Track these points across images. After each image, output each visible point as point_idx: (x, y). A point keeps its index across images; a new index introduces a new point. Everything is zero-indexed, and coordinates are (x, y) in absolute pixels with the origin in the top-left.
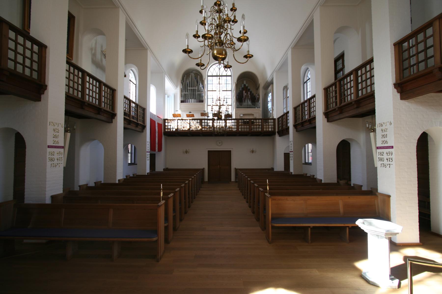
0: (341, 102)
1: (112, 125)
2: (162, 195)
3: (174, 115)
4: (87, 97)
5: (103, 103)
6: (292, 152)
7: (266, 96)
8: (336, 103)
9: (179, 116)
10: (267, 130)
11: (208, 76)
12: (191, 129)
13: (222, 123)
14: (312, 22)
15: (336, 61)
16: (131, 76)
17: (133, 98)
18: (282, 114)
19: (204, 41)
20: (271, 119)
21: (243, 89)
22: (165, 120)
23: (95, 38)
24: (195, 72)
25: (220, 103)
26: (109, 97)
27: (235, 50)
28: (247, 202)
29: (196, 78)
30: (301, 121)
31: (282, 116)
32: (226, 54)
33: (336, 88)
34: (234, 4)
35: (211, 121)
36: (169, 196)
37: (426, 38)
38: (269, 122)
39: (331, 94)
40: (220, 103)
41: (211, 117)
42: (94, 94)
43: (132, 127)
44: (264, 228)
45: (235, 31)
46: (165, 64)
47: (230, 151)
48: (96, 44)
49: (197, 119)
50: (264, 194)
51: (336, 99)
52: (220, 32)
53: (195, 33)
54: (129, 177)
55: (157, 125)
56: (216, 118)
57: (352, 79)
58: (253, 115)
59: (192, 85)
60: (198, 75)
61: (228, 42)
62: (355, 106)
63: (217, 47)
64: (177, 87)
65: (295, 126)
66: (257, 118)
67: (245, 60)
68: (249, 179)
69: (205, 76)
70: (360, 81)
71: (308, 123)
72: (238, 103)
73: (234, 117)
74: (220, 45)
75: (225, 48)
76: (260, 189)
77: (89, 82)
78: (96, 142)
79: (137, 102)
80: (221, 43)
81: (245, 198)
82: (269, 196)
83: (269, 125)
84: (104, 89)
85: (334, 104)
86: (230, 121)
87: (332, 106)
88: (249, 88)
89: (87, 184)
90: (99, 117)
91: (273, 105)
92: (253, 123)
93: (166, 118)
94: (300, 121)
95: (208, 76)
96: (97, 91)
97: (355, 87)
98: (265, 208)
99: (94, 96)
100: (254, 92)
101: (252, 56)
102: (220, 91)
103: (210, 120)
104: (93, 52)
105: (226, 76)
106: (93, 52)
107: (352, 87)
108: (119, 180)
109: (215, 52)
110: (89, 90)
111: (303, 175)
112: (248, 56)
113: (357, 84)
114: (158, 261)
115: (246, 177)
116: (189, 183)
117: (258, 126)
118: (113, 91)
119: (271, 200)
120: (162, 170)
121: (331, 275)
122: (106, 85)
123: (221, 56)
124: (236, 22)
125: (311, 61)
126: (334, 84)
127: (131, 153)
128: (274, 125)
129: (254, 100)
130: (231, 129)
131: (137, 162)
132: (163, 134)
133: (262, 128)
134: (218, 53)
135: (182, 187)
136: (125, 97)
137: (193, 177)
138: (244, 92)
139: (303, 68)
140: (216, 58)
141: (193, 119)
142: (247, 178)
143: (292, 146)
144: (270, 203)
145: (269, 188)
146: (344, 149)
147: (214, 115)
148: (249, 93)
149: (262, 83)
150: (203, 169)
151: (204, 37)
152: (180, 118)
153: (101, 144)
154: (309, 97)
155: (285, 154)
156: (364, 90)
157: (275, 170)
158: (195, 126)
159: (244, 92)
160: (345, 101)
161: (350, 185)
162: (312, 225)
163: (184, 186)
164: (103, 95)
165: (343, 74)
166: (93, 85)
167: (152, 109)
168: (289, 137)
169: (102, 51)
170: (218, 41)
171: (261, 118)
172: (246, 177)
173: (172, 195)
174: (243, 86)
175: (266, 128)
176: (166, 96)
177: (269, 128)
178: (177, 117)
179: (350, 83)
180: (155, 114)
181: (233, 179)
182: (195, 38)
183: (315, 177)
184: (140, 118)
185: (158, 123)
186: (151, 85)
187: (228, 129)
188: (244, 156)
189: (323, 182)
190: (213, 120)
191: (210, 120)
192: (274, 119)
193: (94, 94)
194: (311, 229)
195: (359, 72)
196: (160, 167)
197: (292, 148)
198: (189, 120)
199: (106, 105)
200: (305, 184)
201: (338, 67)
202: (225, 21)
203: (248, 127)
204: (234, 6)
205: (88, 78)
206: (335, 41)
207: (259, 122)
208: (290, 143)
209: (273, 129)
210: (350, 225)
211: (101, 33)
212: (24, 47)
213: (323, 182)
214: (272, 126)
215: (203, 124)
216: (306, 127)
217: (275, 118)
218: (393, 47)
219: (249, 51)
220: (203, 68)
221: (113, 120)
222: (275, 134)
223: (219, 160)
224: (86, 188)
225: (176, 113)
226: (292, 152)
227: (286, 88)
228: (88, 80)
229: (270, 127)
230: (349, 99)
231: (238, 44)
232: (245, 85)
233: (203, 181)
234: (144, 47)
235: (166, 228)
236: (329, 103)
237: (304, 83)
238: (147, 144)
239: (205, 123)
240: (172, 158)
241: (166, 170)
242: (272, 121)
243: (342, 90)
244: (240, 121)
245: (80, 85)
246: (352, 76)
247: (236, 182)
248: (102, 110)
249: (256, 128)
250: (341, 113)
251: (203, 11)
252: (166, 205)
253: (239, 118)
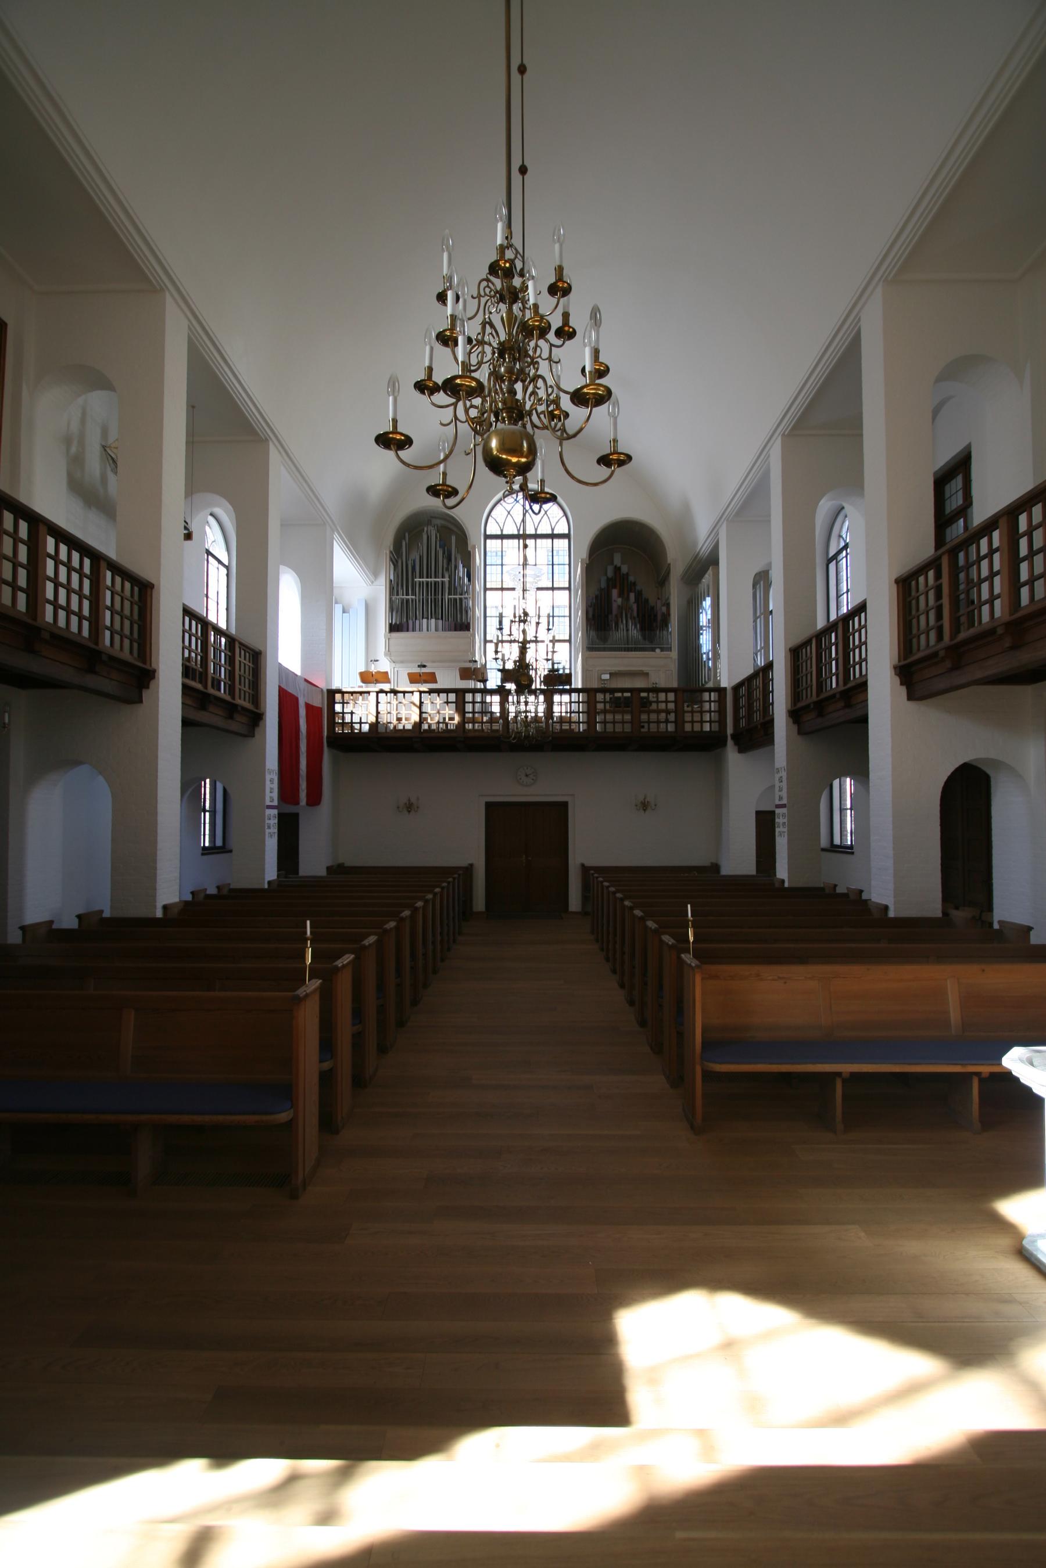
0: (956, 628)
2: (309, 961)
3: (366, 677)
4: (49, 609)
5: (108, 633)
6: (783, 806)
7: (693, 608)
8: (940, 630)
9: (384, 677)
10: (697, 727)
11: (487, 537)
12: (425, 727)
13: (534, 706)
14: (855, 344)
15: (941, 482)
16: (213, 538)
17: (218, 614)
18: (750, 671)
19: (455, 405)
20: (710, 690)
21: (611, 583)
22: (332, 693)
23: (80, 401)
24: (439, 522)
25: (524, 632)
26: (127, 611)
27: (565, 436)
28: (622, 986)
29: (444, 544)
30: (814, 698)
31: (750, 679)
32: (533, 451)
33: (938, 576)
34: (560, 270)
35: (496, 699)
36: (339, 963)
38: (702, 702)
39: (922, 599)
40: (524, 632)
41: (494, 680)
42: (75, 598)
43: (212, 717)
44: (678, 1078)
45: (565, 367)
46: (331, 496)
47: (565, 805)
48: (83, 421)
49: (447, 691)
50: (679, 958)
51: (939, 616)
52: (510, 371)
53: (421, 376)
54: (202, 895)
55: (302, 712)
56: (511, 686)
57: (996, 544)
58: (647, 674)
59: (429, 572)
60: (450, 531)
61: (541, 408)
62: (1007, 642)
63: (500, 425)
64: (376, 574)
65: (795, 715)
66: (662, 684)
67: (604, 471)
68: (627, 903)
69: (475, 538)
70: (1023, 551)
71: (841, 704)
72: (593, 633)
73: (578, 682)
74: (510, 418)
75: (529, 426)
76: (666, 938)
77: (56, 558)
78: (84, 770)
79: (233, 631)
80: (516, 412)
81: (614, 972)
82: (694, 963)
83: (702, 712)
84: (109, 583)
85: (933, 635)
86: (566, 698)
87: (927, 643)
88: (631, 578)
89: (51, 922)
90: (91, 681)
91: (716, 640)
92: (645, 703)
93: (336, 685)
94: (811, 697)
95: (487, 537)
96: (86, 590)
97: (1005, 572)
98: (681, 1007)
99: (75, 607)
100: (650, 594)
101: (629, 458)
102: (529, 590)
103: (492, 692)
104: (74, 449)
105: (552, 536)
106: (74, 449)
107: (998, 573)
108: (165, 908)
109: (494, 443)
110: (57, 585)
111: (822, 889)
112: (613, 460)
113: (1014, 561)
114: (294, 1196)
115: (619, 895)
116: (413, 917)
117: (663, 716)
118: (143, 591)
119: (703, 979)
120: (323, 872)
121: (912, 1247)
122: (117, 569)
123: (514, 460)
124: (572, 335)
125: (851, 479)
126: (934, 564)
127: (213, 812)
128: (722, 711)
129: (651, 623)
130: (566, 727)
131: (234, 843)
132: (324, 741)
133: (679, 722)
134: (503, 448)
135: (386, 931)
136: (187, 612)
137: (430, 896)
138: (615, 593)
139: (825, 506)
140: (496, 466)
141: (431, 692)
142: (622, 900)
143: (784, 784)
144: (698, 987)
145: (695, 935)
146: (967, 796)
147: (506, 675)
148: (632, 596)
149: (677, 561)
150: (469, 870)
151: (450, 386)
152: (386, 687)
153: (101, 778)
154: (844, 610)
155: (758, 813)
157: (725, 871)
158: (440, 712)
159: (615, 593)
160: (971, 624)
161: (991, 924)
162: (847, 1068)
163: (397, 928)
164: (108, 603)
165: (966, 528)
166: (70, 569)
167: (288, 653)
168: (773, 751)
169: (104, 447)
170: (504, 402)
171: (675, 685)
172: (619, 895)
173: (348, 958)
174: (610, 573)
175: (692, 722)
176: (338, 609)
177: (702, 722)
178: (377, 682)
179: (989, 560)
180: (298, 671)
181: (575, 903)
182: (423, 393)
183: (864, 896)
184: (243, 686)
185: (308, 706)
186: (283, 568)
187: (558, 727)
188: (613, 823)
189: (891, 914)
190: (502, 692)
191: (492, 692)
192: (721, 691)
193: (75, 598)
194: (844, 1081)
195: (1023, 519)
196: (313, 862)
197: (782, 794)
198: (417, 695)
199: (117, 638)
200: (831, 920)
201: (947, 503)
202: (527, 330)
203: (628, 717)
204: (560, 277)
205: (51, 542)
206: (936, 412)
207: (667, 702)
208: (777, 776)
209: (716, 727)
210: (985, 1069)
211: (101, 383)
213: (891, 914)
214: (715, 716)
215: (469, 708)
216: (833, 717)
217: (723, 685)
219: (615, 441)
220: (451, 502)
221: (146, 694)
222: (724, 744)
223: (527, 837)
224: (49, 934)
225: (373, 669)
226: (783, 806)
227: (762, 580)
228: (50, 548)
229: (707, 717)
230: (986, 617)
231: (577, 414)
232: (617, 569)
233: (466, 912)
234: (257, 434)
235: (327, 1079)
236: (914, 631)
237: (829, 561)
238: (268, 777)
239: (474, 703)
240: (354, 829)
241: (337, 870)
242: (714, 696)
243: (962, 587)
244: (600, 697)
245: (23, 566)
246: (996, 535)
247: (584, 913)
248: (104, 658)
249: (658, 722)
250: (956, 667)
251: (450, 294)
252: (327, 995)
253: (595, 685)
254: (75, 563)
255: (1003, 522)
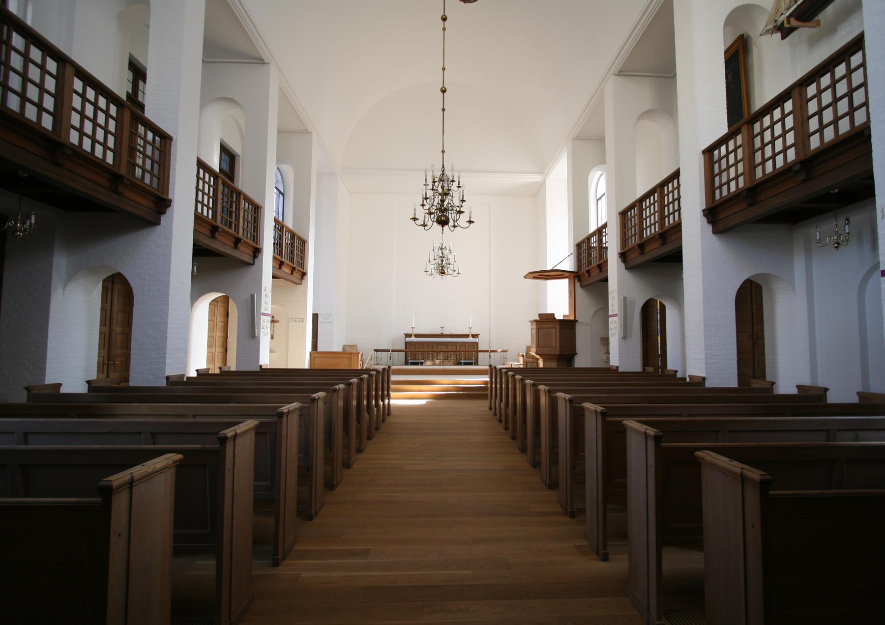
1: (253, 268)
37: (834, 83)
65: (623, 256)
70: (716, 171)
94: (634, 241)
97: (746, 160)
156: (725, 188)
189: (620, 370)
212: (94, 124)
218: (702, 156)
221: (163, 219)
254: (207, 179)
255: (795, 93)
